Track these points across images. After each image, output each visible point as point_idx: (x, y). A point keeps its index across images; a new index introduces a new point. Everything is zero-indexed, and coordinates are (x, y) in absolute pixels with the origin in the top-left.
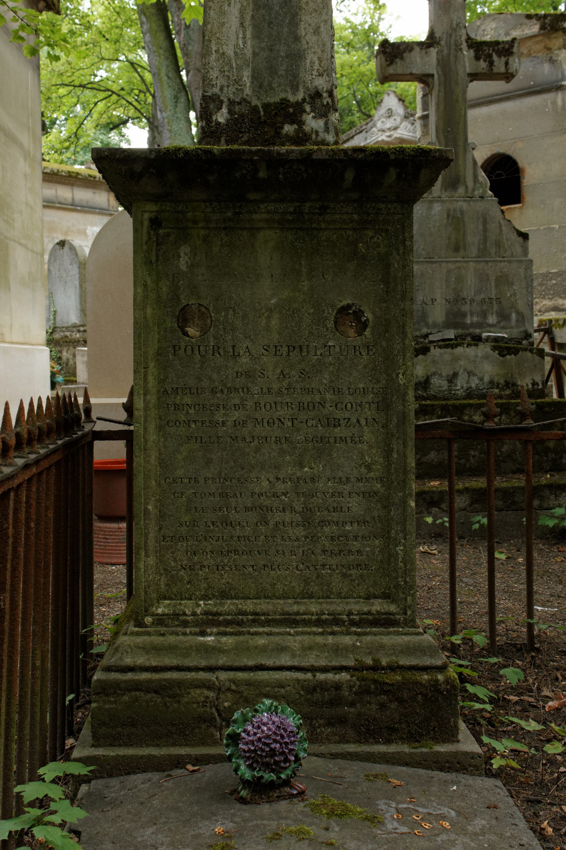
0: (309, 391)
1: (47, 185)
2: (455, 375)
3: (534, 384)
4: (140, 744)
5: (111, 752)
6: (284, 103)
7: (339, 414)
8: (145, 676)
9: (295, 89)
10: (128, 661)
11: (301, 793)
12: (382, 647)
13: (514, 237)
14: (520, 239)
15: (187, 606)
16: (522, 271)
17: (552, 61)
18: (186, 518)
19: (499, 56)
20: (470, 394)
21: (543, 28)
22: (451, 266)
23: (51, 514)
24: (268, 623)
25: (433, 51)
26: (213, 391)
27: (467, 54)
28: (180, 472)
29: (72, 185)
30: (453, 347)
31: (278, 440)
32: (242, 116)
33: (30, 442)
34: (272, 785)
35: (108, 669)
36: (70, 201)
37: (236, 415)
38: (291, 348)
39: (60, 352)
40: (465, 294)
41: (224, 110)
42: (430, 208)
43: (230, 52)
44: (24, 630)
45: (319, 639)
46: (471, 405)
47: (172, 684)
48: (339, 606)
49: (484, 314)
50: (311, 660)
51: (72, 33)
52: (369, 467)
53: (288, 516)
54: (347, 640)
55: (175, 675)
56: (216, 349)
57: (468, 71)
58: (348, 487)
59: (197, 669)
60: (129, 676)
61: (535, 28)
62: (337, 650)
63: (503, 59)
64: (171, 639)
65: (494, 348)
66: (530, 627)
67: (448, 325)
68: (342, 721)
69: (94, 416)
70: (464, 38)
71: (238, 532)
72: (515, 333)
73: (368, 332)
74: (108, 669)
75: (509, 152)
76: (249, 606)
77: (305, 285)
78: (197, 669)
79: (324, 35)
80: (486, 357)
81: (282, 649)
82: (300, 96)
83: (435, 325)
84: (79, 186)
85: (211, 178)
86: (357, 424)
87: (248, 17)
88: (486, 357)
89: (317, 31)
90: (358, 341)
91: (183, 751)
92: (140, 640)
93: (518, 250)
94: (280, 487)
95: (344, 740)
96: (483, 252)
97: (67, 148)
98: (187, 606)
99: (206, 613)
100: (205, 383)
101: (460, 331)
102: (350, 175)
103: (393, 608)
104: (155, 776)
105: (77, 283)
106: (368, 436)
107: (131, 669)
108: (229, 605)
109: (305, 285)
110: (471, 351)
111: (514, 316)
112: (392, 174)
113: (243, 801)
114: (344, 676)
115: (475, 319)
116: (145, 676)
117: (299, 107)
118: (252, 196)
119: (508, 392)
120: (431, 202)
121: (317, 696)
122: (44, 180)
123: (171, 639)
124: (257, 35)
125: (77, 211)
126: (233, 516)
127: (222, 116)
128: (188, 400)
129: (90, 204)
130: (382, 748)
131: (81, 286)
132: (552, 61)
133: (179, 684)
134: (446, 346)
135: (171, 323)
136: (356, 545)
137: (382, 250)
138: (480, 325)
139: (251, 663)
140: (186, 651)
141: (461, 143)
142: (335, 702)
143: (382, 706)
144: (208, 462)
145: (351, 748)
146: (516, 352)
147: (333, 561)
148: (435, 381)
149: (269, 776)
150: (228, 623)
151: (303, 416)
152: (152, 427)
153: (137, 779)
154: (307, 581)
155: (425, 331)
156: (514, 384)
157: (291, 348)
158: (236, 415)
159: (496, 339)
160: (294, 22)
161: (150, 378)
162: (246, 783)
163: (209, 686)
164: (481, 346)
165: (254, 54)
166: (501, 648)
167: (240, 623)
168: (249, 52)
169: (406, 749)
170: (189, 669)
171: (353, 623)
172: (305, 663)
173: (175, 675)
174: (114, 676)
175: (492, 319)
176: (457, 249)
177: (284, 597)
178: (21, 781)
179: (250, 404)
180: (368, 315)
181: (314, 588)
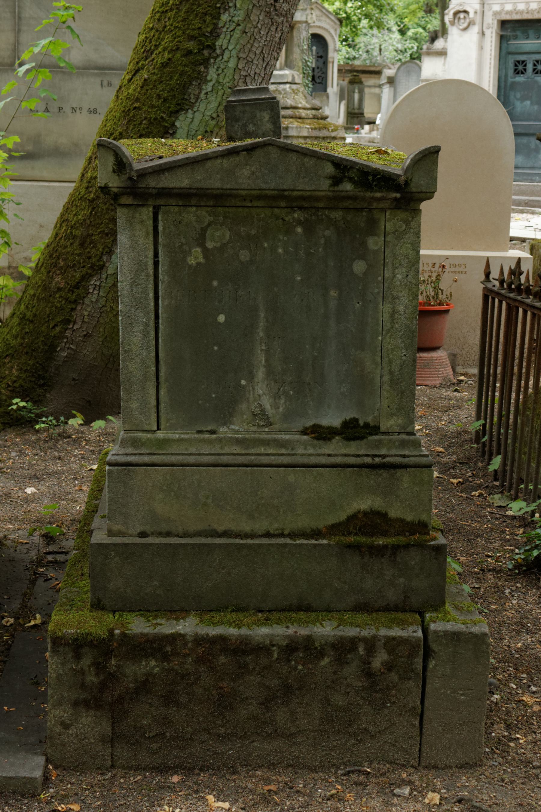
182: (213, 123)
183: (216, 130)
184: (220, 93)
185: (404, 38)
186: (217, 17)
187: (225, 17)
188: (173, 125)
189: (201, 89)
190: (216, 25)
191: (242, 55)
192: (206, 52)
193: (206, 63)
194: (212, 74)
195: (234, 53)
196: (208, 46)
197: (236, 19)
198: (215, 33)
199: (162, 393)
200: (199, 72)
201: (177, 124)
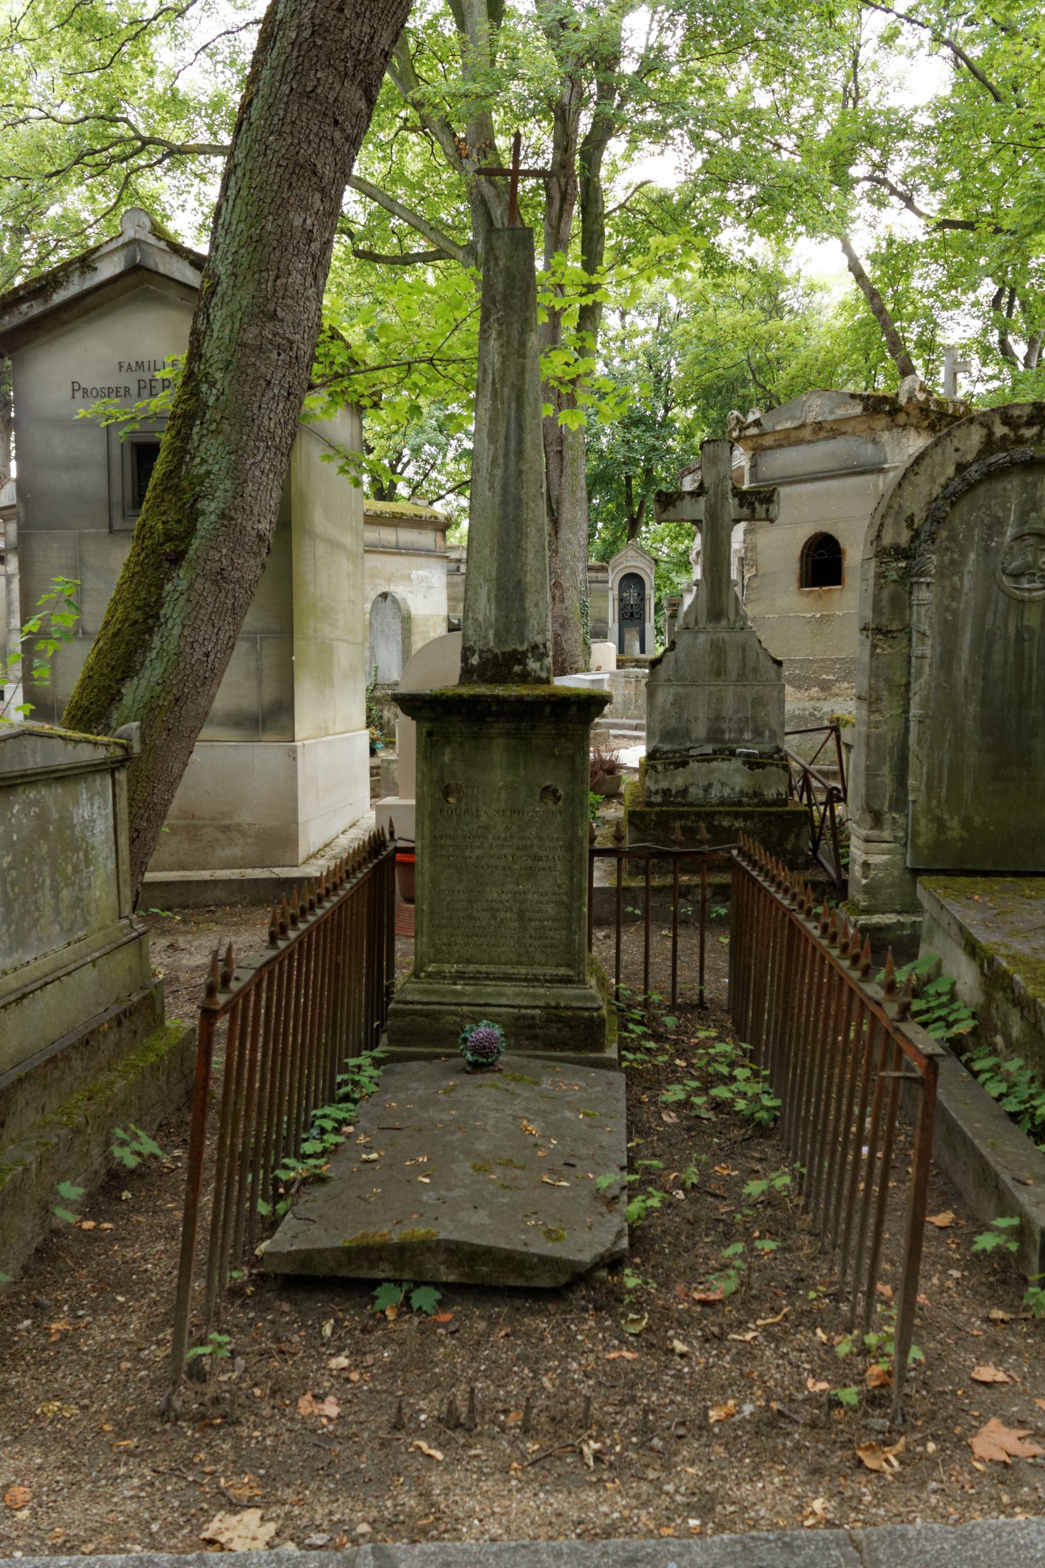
0: (524, 838)
1: (368, 527)
2: (710, 785)
3: (779, 794)
4: (416, 1045)
5: (398, 1049)
6: (515, 652)
7: (542, 853)
8: (419, 1007)
9: (522, 643)
10: (410, 998)
11: (500, 1070)
12: (562, 995)
13: (770, 663)
14: (775, 666)
15: (446, 968)
16: (775, 694)
17: (875, 442)
18: (447, 914)
19: (761, 504)
20: (722, 803)
21: (865, 409)
22: (713, 689)
23: (365, 910)
24: (495, 979)
25: (702, 500)
26: (464, 838)
27: (732, 502)
28: (443, 887)
29: (396, 526)
30: (709, 761)
31: (504, 868)
32: (488, 660)
33: (354, 871)
34: (483, 1065)
35: (398, 1002)
36: (394, 543)
37: (478, 852)
38: (513, 812)
39: (381, 710)
40: (724, 714)
41: (476, 656)
42: (696, 638)
43: (481, 618)
44: (237, 1226)
45: (525, 990)
46: (720, 812)
47: (435, 1012)
48: (538, 970)
49: (741, 731)
50: (519, 1001)
51: (398, 393)
52: (559, 886)
53: (509, 915)
54: (542, 991)
55: (437, 1007)
56: (467, 812)
57: (733, 517)
58: (546, 899)
59: (450, 1004)
60: (410, 1006)
61: (858, 409)
62: (534, 996)
63: (764, 507)
64: (436, 986)
65: (745, 763)
66: (701, 992)
67: (709, 740)
68: (535, 1037)
69: (396, 836)
70: (730, 487)
71: (478, 923)
72: (767, 748)
73: (560, 803)
74: (398, 1002)
75: (832, 532)
76: (484, 968)
77: (522, 772)
78: (450, 1004)
79: (541, 607)
80: (737, 770)
81: (501, 995)
82: (525, 647)
83: (697, 740)
84: (404, 527)
85: (463, 710)
86: (903, 689)
87: (493, 595)
88: (737, 770)
89: (537, 605)
90: (555, 808)
91: (440, 1050)
92: (417, 986)
93: (773, 675)
94: (504, 897)
95: (536, 1048)
96: (742, 676)
97: (396, 432)
98: (446, 968)
99: (458, 972)
100: (459, 832)
101: (718, 746)
102: (548, 709)
103: (571, 973)
104: (423, 1063)
105: (399, 638)
106: (559, 867)
107: (411, 1003)
108: (472, 968)
109: (522, 772)
110: (724, 765)
111: (767, 733)
112: (574, 709)
113: (468, 1072)
114: (538, 1011)
115: (733, 735)
116: (419, 1007)
117: (524, 655)
118: (489, 719)
119: (756, 801)
120: (697, 632)
121: (520, 1023)
122: (365, 523)
123: (436, 986)
124: (499, 607)
125: (401, 554)
126: (475, 914)
127: (475, 660)
128: (448, 842)
129: (416, 546)
130: (558, 1054)
131: (403, 642)
132: (875, 442)
133: (439, 1012)
134: (703, 761)
135: (439, 795)
136: (551, 934)
137: (571, 751)
138: (736, 741)
139: (482, 1002)
140: (444, 994)
141: (724, 581)
142: (532, 1026)
143: (560, 1029)
144: (461, 880)
145: (540, 1053)
146: (763, 766)
147: (536, 943)
148: (692, 790)
149: (482, 1060)
150: (470, 978)
151: (519, 854)
152: (426, 859)
153: (414, 1065)
154: (520, 955)
155: (688, 745)
156: (761, 794)
157: (513, 812)
158: (478, 852)
159: (748, 755)
160: (522, 599)
161: (426, 830)
162: (469, 1063)
163: (457, 1014)
164: (734, 760)
165: (497, 620)
166: (680, 1006)
167: (478, 979)
168: (493, 619)
169: (572, 1054)
170: (445, 1004)
171: (547, 981)
172: (515, 1003)
173: (437, 1007)
174: (401, 1006)
175: (747, 736)
176: (718, 674)
177: (506, 964)
178: (347, 1057)
179: (487, 846)
180: (561, 792)
181: (524, 959)
182: (160, 688)
183: (163, 695)
184: (165, 660)
185: (789, 352)
186: (162, 588)
187: (168, 587)
188: (119, 692)
189: (145, 656)
190: (159, 595)
191: (186, 622)
192: (151, 621)
193: (150, 631)
194: (156, 642)
195: (178, 621)
196: (152, 616)
197: (179, 588)
198: (159, 603)
199: (423, 1231)
200: (144, 641)
201: (123, 691)
